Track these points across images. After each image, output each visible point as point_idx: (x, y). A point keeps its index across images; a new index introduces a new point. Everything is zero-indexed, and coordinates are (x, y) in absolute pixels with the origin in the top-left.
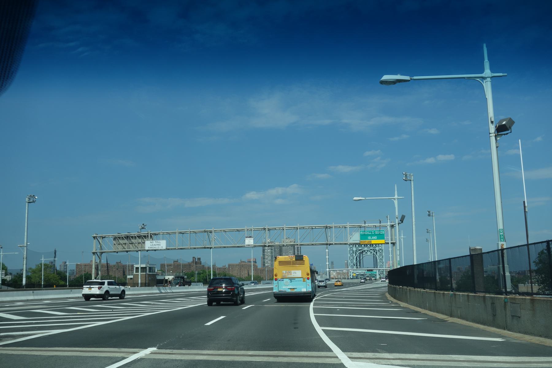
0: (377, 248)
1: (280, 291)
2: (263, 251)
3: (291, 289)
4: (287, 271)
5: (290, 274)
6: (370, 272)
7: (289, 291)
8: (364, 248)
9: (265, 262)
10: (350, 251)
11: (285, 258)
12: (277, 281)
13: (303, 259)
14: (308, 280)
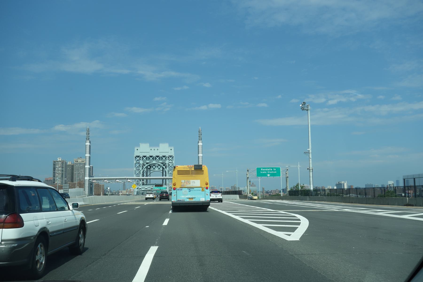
0: (167, 162)
1: (178, 201)
2: (53, 169)
3: (189, 198)
4: (186, 181)
5: (188, 183)
6: (158, 187)
7: (188, 200)
8: (152, 161)
9: (55, 180)
10: (136, 164)
11: (184, 167)
12: (176, 190)
13: (202, 169)
14: (207, 190)
